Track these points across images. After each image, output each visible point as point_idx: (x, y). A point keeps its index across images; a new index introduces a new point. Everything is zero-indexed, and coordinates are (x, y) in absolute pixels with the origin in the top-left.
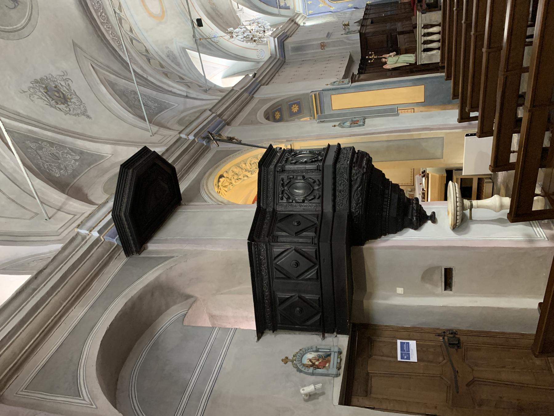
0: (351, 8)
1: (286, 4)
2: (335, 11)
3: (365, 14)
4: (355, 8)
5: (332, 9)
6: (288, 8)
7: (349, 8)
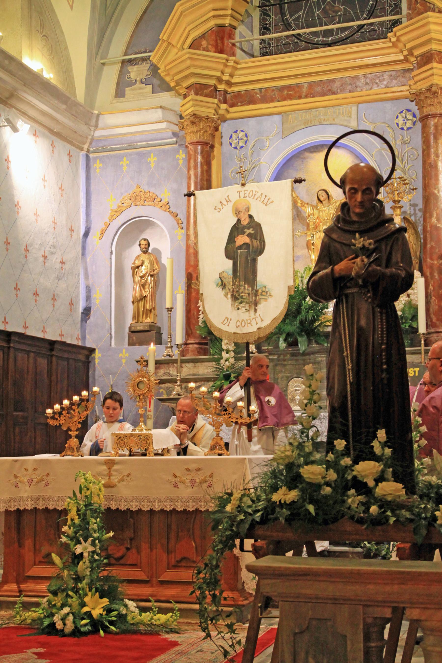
0: (88, 298)
1: (131, 84)
2: (89, 247)
3: (52, 343)
4: (87, 312)
5: (94, 237)
6: (120, 93)
7: (89, 290)
